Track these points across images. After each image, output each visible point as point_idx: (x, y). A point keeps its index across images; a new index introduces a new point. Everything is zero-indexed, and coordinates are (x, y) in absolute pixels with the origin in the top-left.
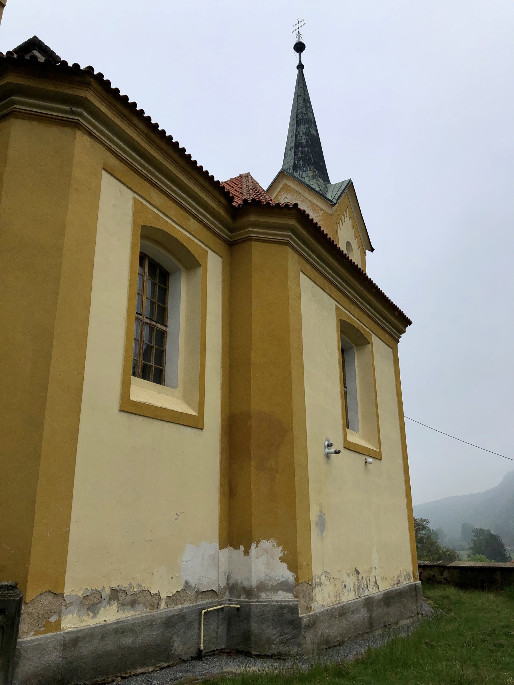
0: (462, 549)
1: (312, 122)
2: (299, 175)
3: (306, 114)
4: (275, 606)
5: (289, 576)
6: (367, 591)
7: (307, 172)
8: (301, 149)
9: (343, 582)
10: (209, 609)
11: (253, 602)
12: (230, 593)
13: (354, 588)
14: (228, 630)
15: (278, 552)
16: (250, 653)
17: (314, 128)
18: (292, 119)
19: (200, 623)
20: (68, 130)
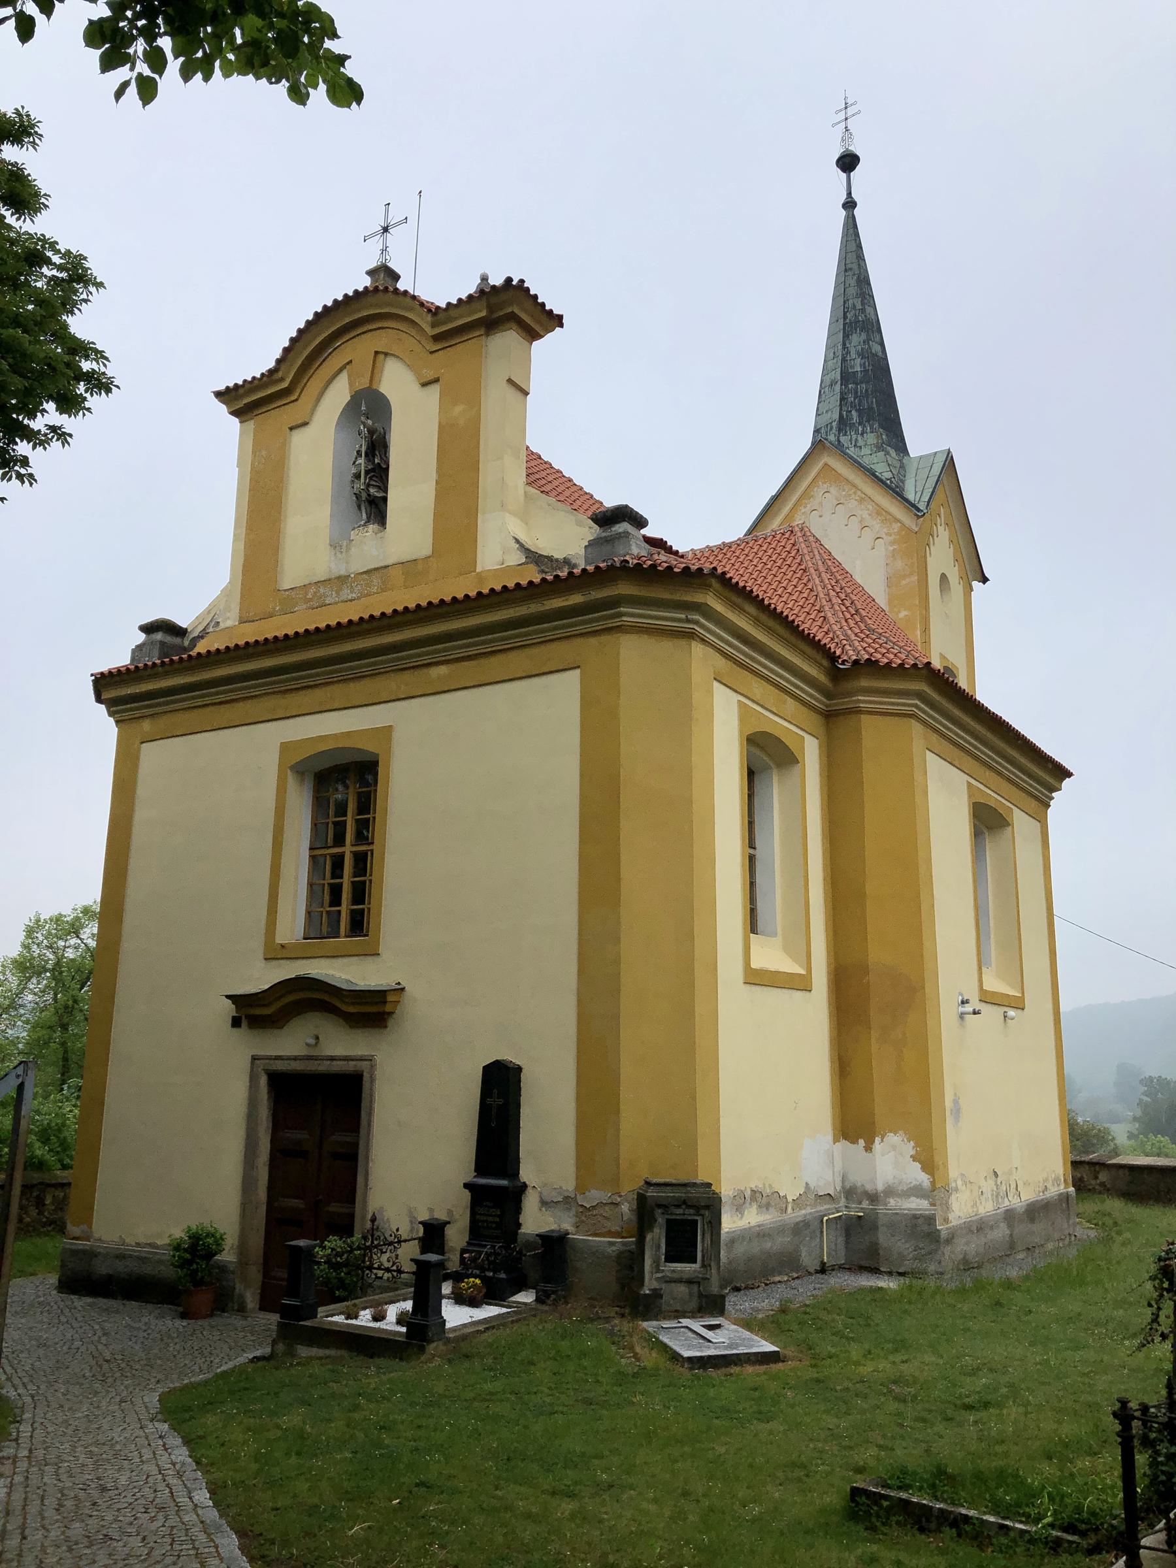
0: (1117, 1120)
1: (872, 328)
2: (851, 440)
3: (863, 310)
4: (906, 1214)
5: (924, 1179)
6: (1006, 1199)
7: (865, 435)
8: (854, 386)
9: (979, 1187)
10: (831, 1217)
11: (880, 1209)
12: (847, 1198)
13: (992, 1195)
14: (847, 1242)
15: (909, 1149)
17: (878, 339)
19: (822, 1232)
20: (683, 642)
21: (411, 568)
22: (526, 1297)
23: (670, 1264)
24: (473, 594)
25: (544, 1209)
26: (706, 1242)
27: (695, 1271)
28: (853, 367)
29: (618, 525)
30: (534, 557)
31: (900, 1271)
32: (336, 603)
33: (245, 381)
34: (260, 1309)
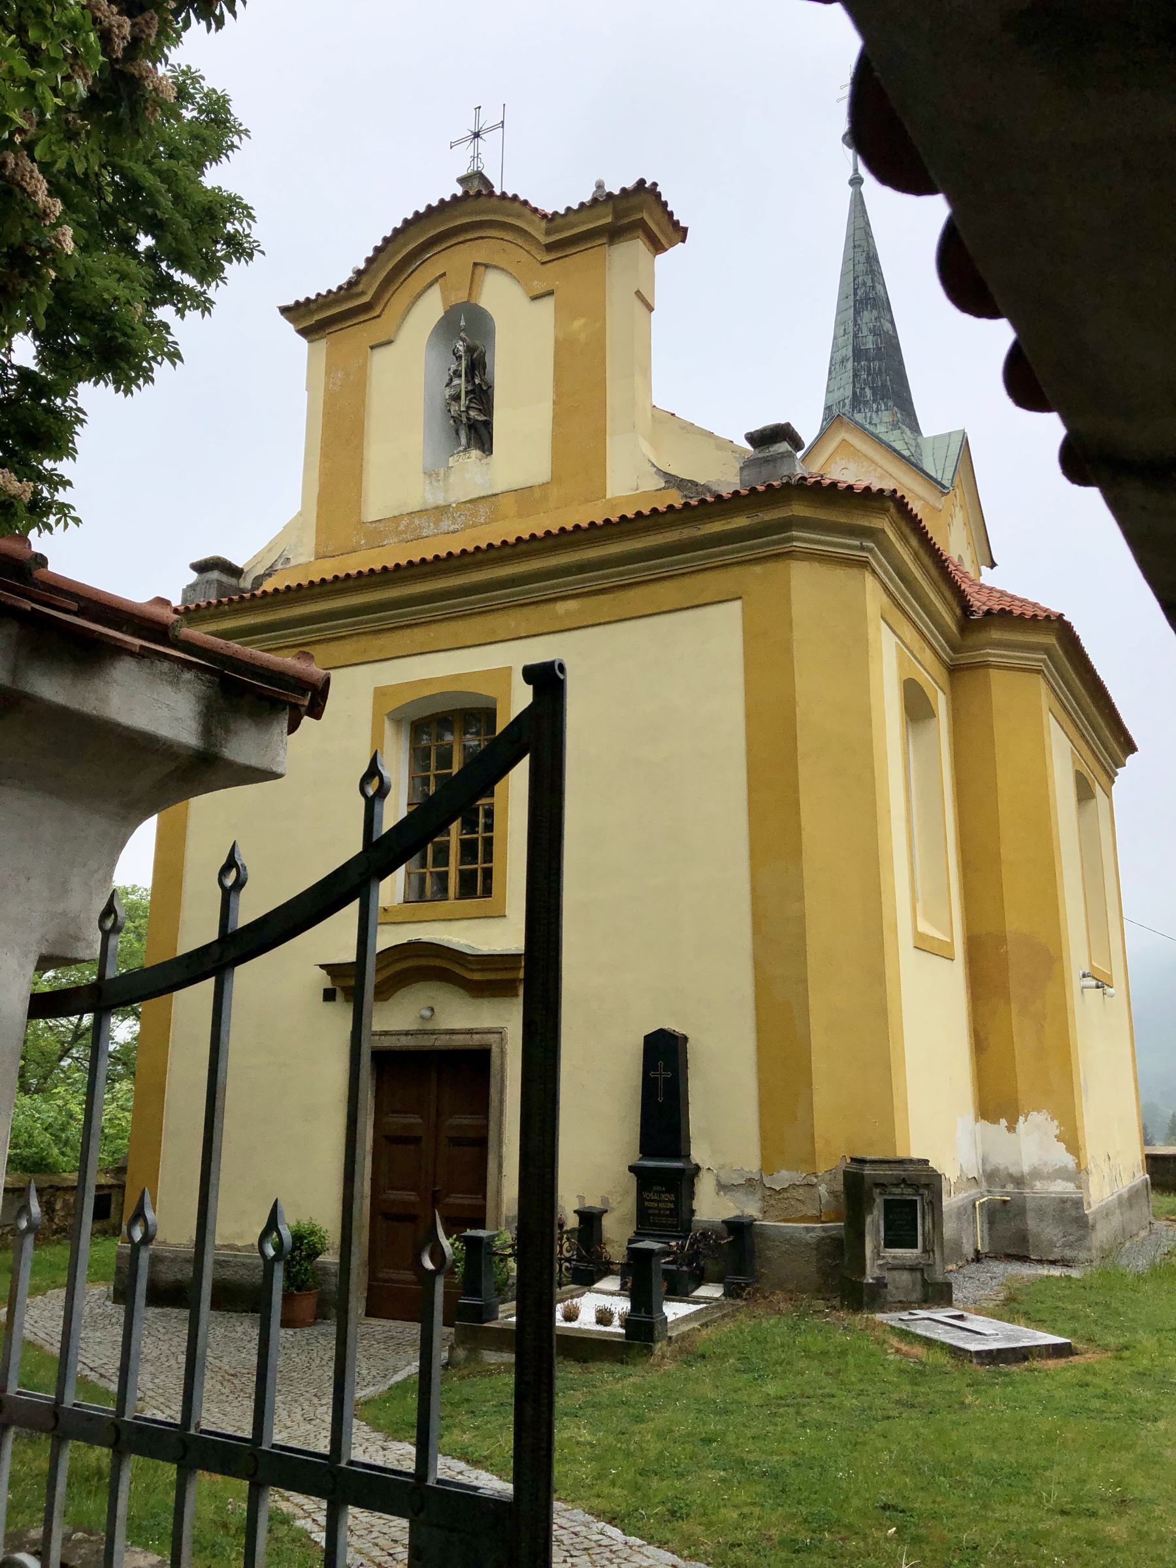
2: (865, 418)
3: (873, 287)
5: (1069, 1161)
14: (990, 1229)
15: (1053, 1128)
16: (1028, 1258)
17: (888, 317)
18: (843, 296)
20: (854, 572)
21: (525, 496)
22: (711, 1291)
23: (890, 1250)
24: (599, 522)
25: (722, 1193)
26: (927, 1224)
27: (917, 1258)
28: (865, 344)
29: (778, 445)
30: (672, 481)
31: (1051, 1258)
32: (435, 535)
33: (319, 295)
34: (367, 1315)
